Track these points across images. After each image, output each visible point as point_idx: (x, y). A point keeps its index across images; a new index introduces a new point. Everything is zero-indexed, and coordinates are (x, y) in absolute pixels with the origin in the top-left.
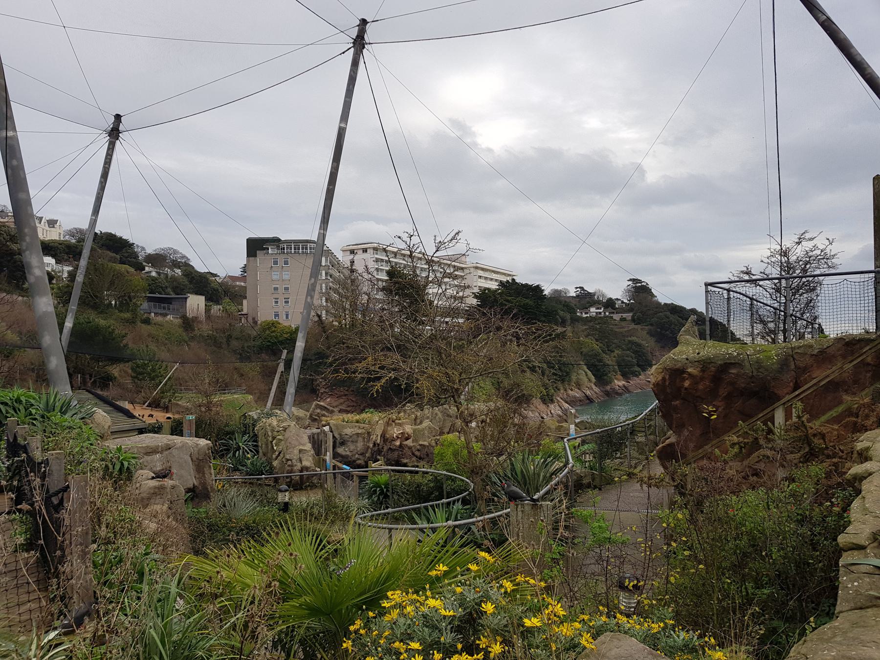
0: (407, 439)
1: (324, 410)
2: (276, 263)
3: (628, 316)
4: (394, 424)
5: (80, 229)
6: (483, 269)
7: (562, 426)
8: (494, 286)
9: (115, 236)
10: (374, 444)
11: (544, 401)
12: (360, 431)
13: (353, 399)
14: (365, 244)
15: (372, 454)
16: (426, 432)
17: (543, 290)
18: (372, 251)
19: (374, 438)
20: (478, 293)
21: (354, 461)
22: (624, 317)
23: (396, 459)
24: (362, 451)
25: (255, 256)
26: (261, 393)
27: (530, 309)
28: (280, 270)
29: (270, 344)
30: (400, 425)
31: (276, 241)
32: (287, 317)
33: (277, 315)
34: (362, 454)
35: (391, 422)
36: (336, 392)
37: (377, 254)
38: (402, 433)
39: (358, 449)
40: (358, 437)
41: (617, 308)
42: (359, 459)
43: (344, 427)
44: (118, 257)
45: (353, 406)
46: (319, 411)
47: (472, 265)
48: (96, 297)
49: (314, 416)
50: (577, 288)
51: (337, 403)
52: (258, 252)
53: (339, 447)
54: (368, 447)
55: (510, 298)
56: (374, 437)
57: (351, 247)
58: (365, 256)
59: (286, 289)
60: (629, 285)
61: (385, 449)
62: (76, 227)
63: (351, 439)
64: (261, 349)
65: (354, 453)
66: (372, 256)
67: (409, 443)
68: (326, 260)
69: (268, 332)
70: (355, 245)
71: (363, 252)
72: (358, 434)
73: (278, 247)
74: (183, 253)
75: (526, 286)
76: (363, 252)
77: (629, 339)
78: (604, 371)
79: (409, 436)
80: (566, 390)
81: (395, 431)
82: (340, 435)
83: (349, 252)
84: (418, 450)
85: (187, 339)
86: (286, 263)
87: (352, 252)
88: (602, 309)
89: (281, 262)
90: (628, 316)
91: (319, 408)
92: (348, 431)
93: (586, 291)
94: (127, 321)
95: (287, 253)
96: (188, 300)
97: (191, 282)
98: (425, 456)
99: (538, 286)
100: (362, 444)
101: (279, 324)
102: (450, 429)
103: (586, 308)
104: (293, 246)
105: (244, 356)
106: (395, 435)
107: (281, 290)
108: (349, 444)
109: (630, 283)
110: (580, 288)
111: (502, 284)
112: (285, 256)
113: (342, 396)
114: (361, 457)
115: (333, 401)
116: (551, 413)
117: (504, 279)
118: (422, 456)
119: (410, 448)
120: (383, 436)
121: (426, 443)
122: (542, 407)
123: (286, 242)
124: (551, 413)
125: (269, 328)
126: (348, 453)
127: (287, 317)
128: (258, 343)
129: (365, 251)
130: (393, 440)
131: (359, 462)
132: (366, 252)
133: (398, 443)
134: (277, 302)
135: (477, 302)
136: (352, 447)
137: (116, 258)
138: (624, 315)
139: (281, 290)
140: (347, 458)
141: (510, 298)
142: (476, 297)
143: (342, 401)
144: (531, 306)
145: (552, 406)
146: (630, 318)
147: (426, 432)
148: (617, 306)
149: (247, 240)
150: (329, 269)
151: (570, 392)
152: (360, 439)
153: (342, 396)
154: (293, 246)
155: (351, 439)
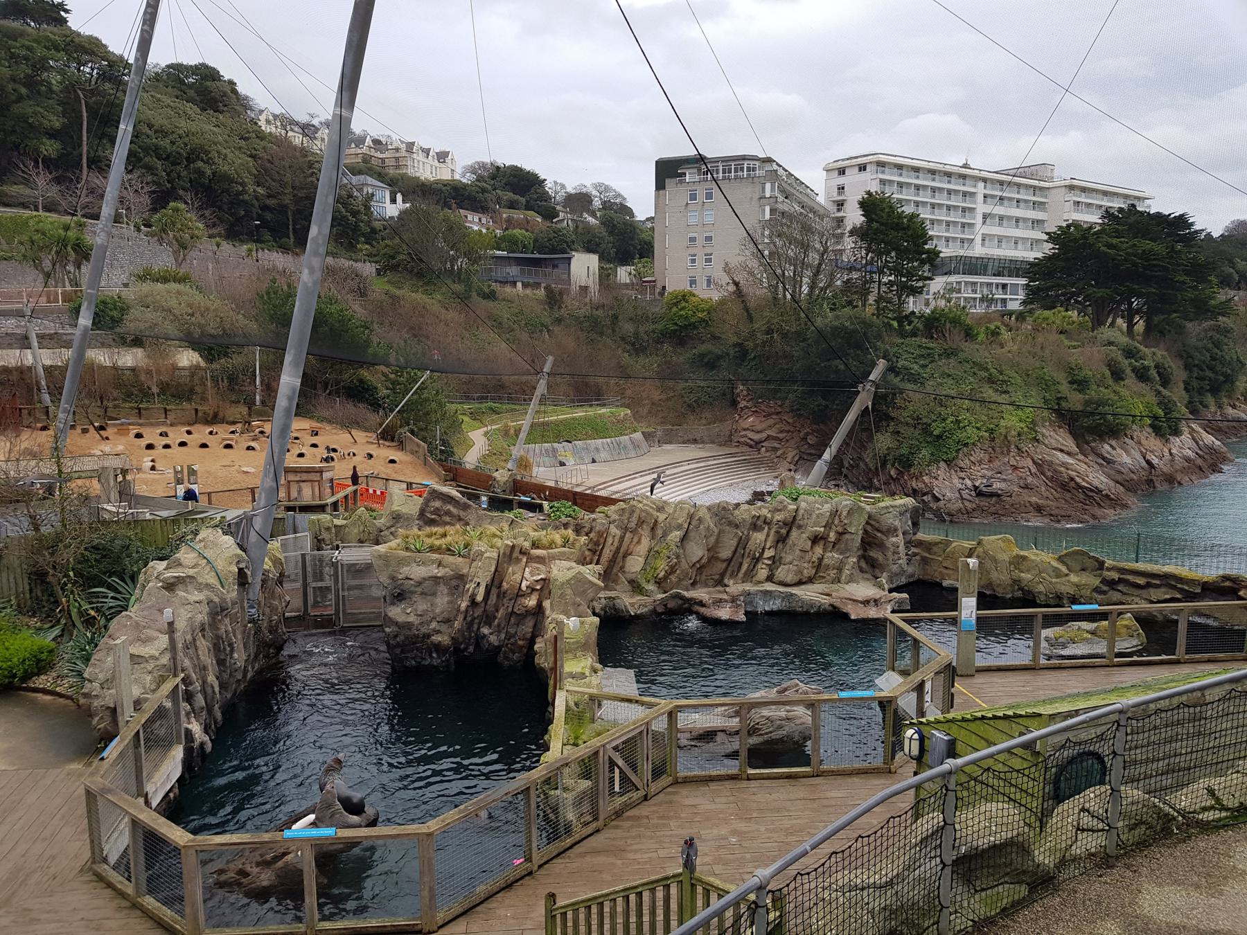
1: (450, 503)
2: (693, 197)
6: (1084, 190)
7: (1024, 558)
8: (1094, 218)
9: (521, 169)
10: (473, 603)
11: (1157, 430)
12: (440, 572)
13: (790, 421)
17: (1192, 224)
18: (874, 167)
20: (1054, 233)
21: (429, 636)
25: (664, 188)
26: (653, 404)
27: (1155, 259)
28: (700, 208)
29: (676, 327)
30: (540, 560)
31: (699, 160)
33: (693, 282)
34: (448, 621)
35: (516, 554)
36: (763, 408)
37: (883, 172)
39: (437, 611)
42: (438, 632)
43: (402, 562)
44: (523, 200)
45: (789, 431)
46: (437, 504)
47: (1063, 183)
48: (421, 260)
49: (428, 515)
51: (763, 425)
55: (1114, 241)
57: (840, 163)
59: (709, 239)
63: (419, 589)
64: (664, 336)
66: (874, 177)
68: (773, 189)
69: (675, 309)
70: (996, 172)
71: (860, 170)
72: (436, 577)
75: (1159, 215)
76: (860, 170)
80: (1220, 407)
83: (837, 172)
85: (548, 321)
87: (842, 171)
91: (439, 499)
92: (418, 572)
94: (457, 295)
96: (573, 262)
97: (611, 233)
99: (1182, 216)
100: (446, 599)
101: (694, 295)
102: (735, 552)
105: (637, 347)
107: (700, 242)
108: (416, 598)
111: (1108, 214)
113: (772, 414)
114: (444, 628)
115: (757, 422)
116: (1171, 454)
117: (1116, 204)
122: (1153, 443)
124: (1171, 454)
125: (676, 304)
126: (412, 619)
128: (660, 327)
129: (862, 168)
131: (437, 638)
132: (865, 170)
133: (532, 602)
134: (693, 261)
135: (1053, 248)
136: (422, 606)
137: (517, 202)
139: (700, 242)
140: (410, 629)
141: (1114, 241)
143: (771, 422)
144: (1158, 254)
145: (1176, 441)
151: (1230, 411)
152: (443, 589)
153: (772, 414)
154: (745, 166)
155: (419, 589)
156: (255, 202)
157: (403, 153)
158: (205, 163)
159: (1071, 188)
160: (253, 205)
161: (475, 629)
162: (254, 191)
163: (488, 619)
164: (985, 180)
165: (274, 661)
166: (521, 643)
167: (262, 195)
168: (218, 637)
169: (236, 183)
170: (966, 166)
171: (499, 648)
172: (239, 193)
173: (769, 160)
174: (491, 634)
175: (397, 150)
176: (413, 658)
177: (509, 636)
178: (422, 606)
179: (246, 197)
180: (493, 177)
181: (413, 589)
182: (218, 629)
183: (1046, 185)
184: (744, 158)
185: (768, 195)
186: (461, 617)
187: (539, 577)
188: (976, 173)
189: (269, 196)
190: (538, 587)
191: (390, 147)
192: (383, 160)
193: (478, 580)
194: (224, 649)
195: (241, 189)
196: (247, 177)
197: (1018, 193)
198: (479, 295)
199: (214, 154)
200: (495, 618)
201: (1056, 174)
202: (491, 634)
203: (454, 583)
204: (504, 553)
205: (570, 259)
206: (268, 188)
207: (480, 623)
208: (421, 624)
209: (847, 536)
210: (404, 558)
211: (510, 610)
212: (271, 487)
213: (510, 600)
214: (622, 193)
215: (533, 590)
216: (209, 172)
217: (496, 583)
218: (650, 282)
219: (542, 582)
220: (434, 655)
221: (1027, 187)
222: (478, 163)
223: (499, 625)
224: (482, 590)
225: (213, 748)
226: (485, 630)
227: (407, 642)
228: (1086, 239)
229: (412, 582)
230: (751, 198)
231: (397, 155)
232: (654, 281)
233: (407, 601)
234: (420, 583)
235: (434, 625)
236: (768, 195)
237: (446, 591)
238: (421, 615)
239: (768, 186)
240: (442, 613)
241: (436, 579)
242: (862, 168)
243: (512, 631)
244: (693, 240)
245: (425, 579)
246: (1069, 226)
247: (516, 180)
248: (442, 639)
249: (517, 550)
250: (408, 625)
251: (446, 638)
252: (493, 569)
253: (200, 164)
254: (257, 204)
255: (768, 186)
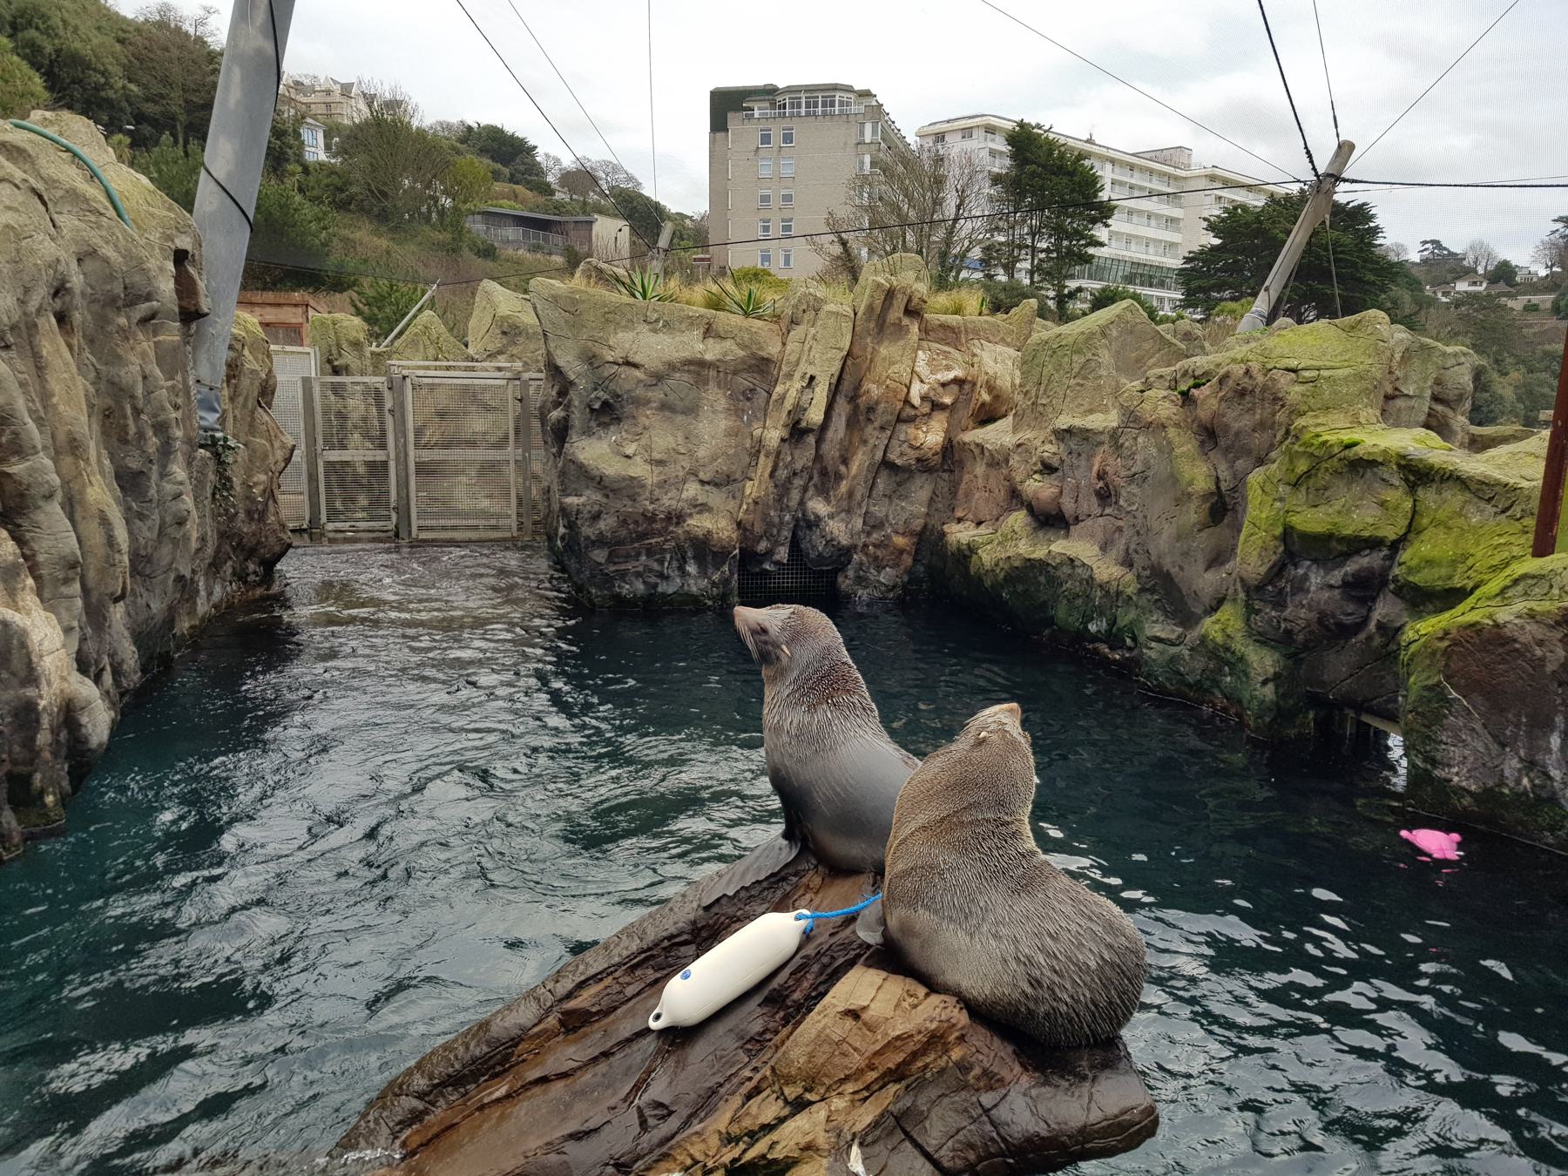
0: (986, 417)
2: (766, 139)
3: (1546, 300)
4: (915, 328)
5: (448, 124)
10: (797, 432)
12: (711, 351)
14: (970, 118)
15: (783, 489)
16: (1105, 357)
17: (1373, 216)
18: (982, 132)
19: (793, 394)
21: (677, 517)
22: (1533, 302)
23: (917, 524)
24: (721, 465)
32: (787, 262)
34: (723, 482)
35: (896, 313)
37: (993, 140)
38: (958, 382)
40: (701, 382)
41: (1518, 284)
42: (703, 508)
44: (506, 171)
47: (1203, 172)
48: (384, 194)
50: (1425, 242)
52: (730, 115)
53: (587, 432)
54: (757, 449)
56: (790, 390)
57: (938, 126)
58: (970, 145)
59: (787, 198)
60: (1553, 232)
61: (860, 462)
62: (441, 119)
65: (676, 470)
67: (998, 435)
68: (874, 132)
72: (702, 364)
73: (773, 105)
74: (630, 171)
77: (1547, 347)
78: (1491, 412)
79: (996, 398)
81: (922, 367)
82: (591, 359)
84: (1048, 469)
86: (788, 138)
88: (1484, 285)
89: (777, 136)
90: (1546, 300)
93: (1445, 249)
94: (440, 246)
95: (792, 116)
96: (596, 228)
98: (1090, 504)
101: (770, 275)
103: (1443, 282)
104: (803, 100)
106: (917, 391)
107: (776, 202)
108: (648, 417)
109: (1559, 225)
110: (1433, 242)
112: (786, 123)
114: (715, 498)
118: (1068, 506)
119: (998, 461)
120: (845, 386)
121: (1105, 420)
123: (790, 90)
126: (639, 469)
127: (787, 262)
130: (905, 416)
131: (699, 524)
133: (932, 436)
138: (1535, 299)
139: (776, 202)
142: (1212, 227)
146: (1549, 305)
147: (1105, 357)
148: (1518, 279)
149: (712, 93)
150: (879, 150)
152: (715, 398)
154: (837, 98)
155: (656, 395)
156: (124, 104)
157: (337, 97)
158: (42, 33)
159: (1213, 178)
160: (122, 110)
161: (793, 503)
162: (124, 87)
163: (825, 478)
164: (1113, 161)
165: (259, 592)
166: (900, 541)
167: (137, 96)
168: (118, 391)
169: (95, 70)
170: (1090, 141)
171: (845, 553)
172: (98, 88)
173: (867, 94)
174: (831, 516)
175: (328, 92)
176: (638, 575)
177: (872, 525)
178: (663, 438)
179: (111, 94)
180: (463, 140)
181: (640, 392)
182: (117, 359)
183: (1183, 174)
184: (835, 88)
185: (868, 139)
186: (764, 464)
187: (951, 375)
188: (1103, 151)
189: (147, 100)
190: (948, 400)
191: (318, 88)
192: (308, 105)
193: (811, 371)
194: (141, 435)
195: (102, 80)
196: (111, 64)
197: (1151, 181)
198: (471, 249)
199: (56, 21)
200: (839, 477)
201: (1194, 160)
202: (831, 516)
203: (743, 382)
204: (870, 308)
205: (591, 223)
206: (146, 87)
207: (805, 489)
208: (663, 483)
209: (1400, 403)
210: (617, 309)
211: (879, 455)
212: (259, 52)
213: (883, 428)
214: (637, 176)
215: (936, 406)
216: (49, 49)
217: (846, 386)
218: (703, 260)
219: (955, 388)
220: (692, 568)
221: (1162, 174)
222: (441, 123)
223: (851, 494)
224: (821, 394)
225: (117, 729)
226: (818, 506)
227: (623, 533)
228: (1261, 223)
229: (638, 373)
230: (845, 144)
231: (328, 100)
232: (709, 259)
233: (625, 425)
234: (658, 378)
235: (692, 490)
236: (868, 139)
237: (723, 403)
238: (660, 463)
239: (868, 127)
240: (714, 459)
241: (698, 367)
242: (967, 133)
243: (879, 510)
244: (765, 199)
245: (672, 367)
246: (1235, 208)
247: (495, 145)
248: (717, 525)
249: (899, 304)
250: (626, 488)
251: (723, 523)
252: (846, 343)
253: (32, 33)
254: (129, 110)
255: (868, 127)
